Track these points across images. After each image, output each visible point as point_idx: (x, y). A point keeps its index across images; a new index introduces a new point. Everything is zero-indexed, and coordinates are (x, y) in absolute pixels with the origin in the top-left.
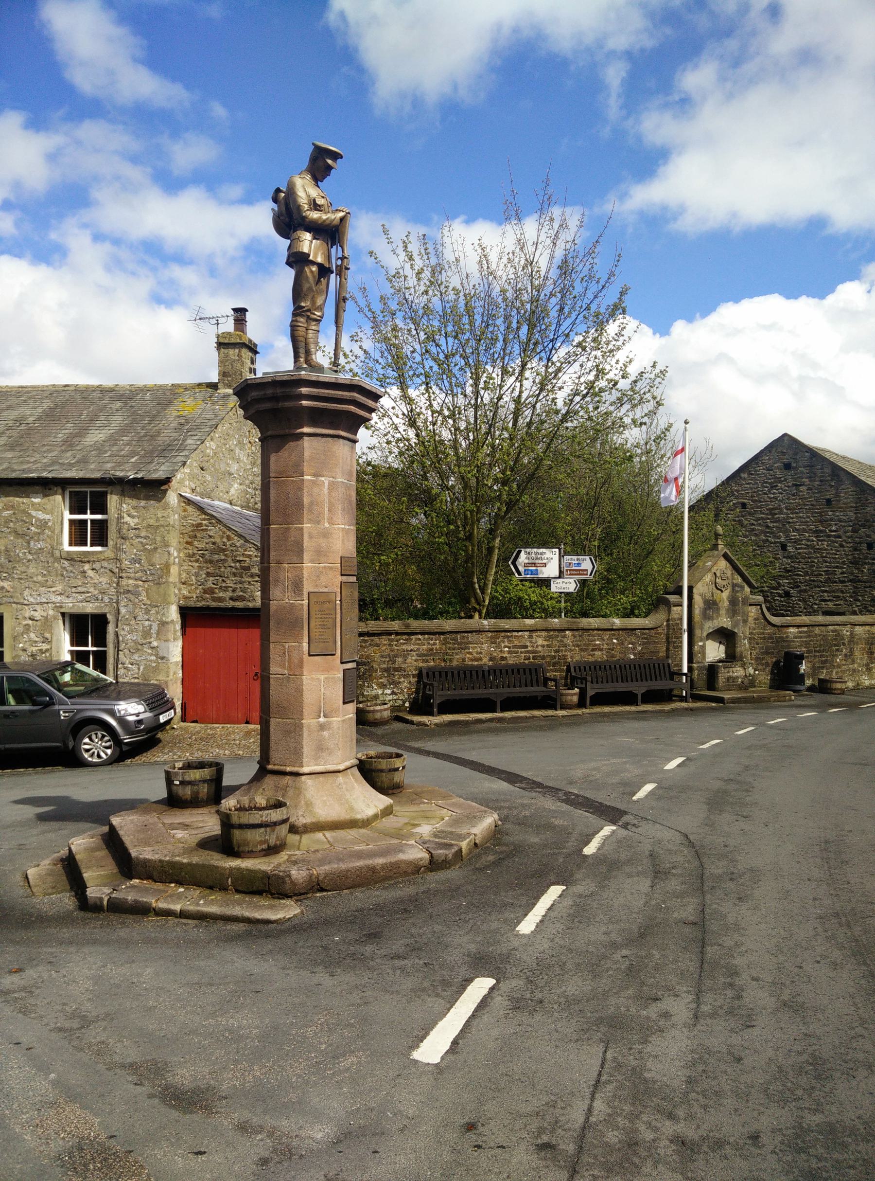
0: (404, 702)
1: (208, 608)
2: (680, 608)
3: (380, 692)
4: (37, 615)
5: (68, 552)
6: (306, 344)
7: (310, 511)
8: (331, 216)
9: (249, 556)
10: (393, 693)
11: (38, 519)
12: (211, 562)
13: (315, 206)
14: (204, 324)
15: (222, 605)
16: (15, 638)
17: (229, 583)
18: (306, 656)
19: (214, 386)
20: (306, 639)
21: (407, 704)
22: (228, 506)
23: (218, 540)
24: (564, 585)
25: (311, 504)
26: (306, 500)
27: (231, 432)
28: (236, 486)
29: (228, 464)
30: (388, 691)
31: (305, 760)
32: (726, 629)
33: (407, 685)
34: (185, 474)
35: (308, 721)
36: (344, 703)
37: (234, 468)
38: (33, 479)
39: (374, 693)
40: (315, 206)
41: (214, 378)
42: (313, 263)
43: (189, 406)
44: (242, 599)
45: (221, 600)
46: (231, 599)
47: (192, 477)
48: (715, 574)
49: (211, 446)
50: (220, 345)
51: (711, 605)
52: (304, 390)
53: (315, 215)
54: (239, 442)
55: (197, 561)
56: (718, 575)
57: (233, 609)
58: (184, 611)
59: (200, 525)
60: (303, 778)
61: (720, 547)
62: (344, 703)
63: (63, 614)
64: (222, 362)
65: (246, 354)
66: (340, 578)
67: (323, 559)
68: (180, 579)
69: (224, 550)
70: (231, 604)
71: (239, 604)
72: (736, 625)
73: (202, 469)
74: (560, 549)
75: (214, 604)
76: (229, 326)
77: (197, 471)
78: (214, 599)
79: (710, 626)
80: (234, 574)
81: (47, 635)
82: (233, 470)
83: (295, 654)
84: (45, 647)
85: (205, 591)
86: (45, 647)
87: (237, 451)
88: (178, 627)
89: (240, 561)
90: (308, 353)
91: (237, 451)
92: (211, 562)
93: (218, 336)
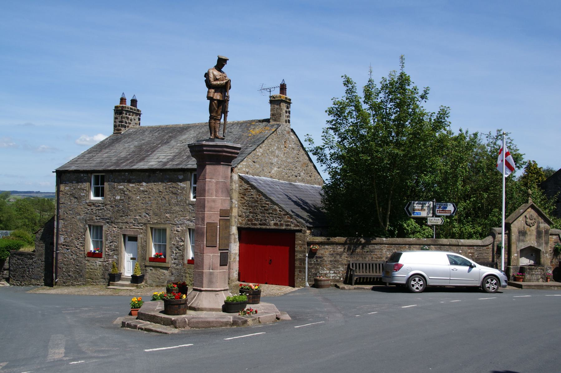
0: (340, 278)
1: (249, 228)
2: (500, 235)
3: (328, 272)
4: (179, 229)
5: (192, 201)
6: (215, 129)
7: (208, 192)
8: (222, 82)
9: (268, 204)
10: (334, 273)
11: (181, 187)
12: (251, 207)
13: (216, 79)
14: (265, 92)
15: (256, 227)
16: (170, 239)
17: (259, 217)
18: (205, 247)
19: (267, 121)
20: (205, 240)
21: (342, 279)
22: (270, 179)
23: (254, 196)
24: (435, 221)
25: (209, 189)
26: (207, 188)
27: (273, 143)
28: (275, 169)
29: (270, 159)
30: (331, 272)
31: (204, 285)
32: (534, 247)
33: (342, 269)
34: (243, 165)
35: (206, 271)
36: (221, 265)
37: (275, 160)
38: (179, 169)
39: (325, 272)
40: (216, 79)
41: (269, 117)
42: (215, 100)
43: (255, 131)
44: (265, 224)
45: (255, 224)
46: (260, 224)
47: (248, 166)
48: (526, 216)
49: (260, 151)
50: (271, 102)
51: (523, 233)
52: (204, 148)
53: (215, 83)
54: (278, 148)
55: (246, 206)
56: (528, 217)
57: (260, 229)
58: (239, 229)
59: (247, 189)
60: (203, 292)
61: (530, 201)
62: (221, 265)
63: (189, 229)
64: (272, 110)
65: (284, 106)
66: (219, 218)
67: (213, 210)
68: (238, 214)
69: (257, 201)
70: (259, 227)
71: (264, 227)
72: (540, 244)
73: (254, 162)
74: (433, 202)
75: (253, 227)
76: (276, 92)
77: (251, 163)
78: (252, 224)
79: (523, 246)
80: (261, 213)
81: (183, 239)
82: (273, 162)
83: (202, 245)
84: (182, 243)
85: (249, 220)
86: (182, 243)
87: (277, 152)
88: (237, 237)
89: (264, 207)
90: (215, 132)
91: (277, 152)
92: (251, 207)
93: (270, 97)
